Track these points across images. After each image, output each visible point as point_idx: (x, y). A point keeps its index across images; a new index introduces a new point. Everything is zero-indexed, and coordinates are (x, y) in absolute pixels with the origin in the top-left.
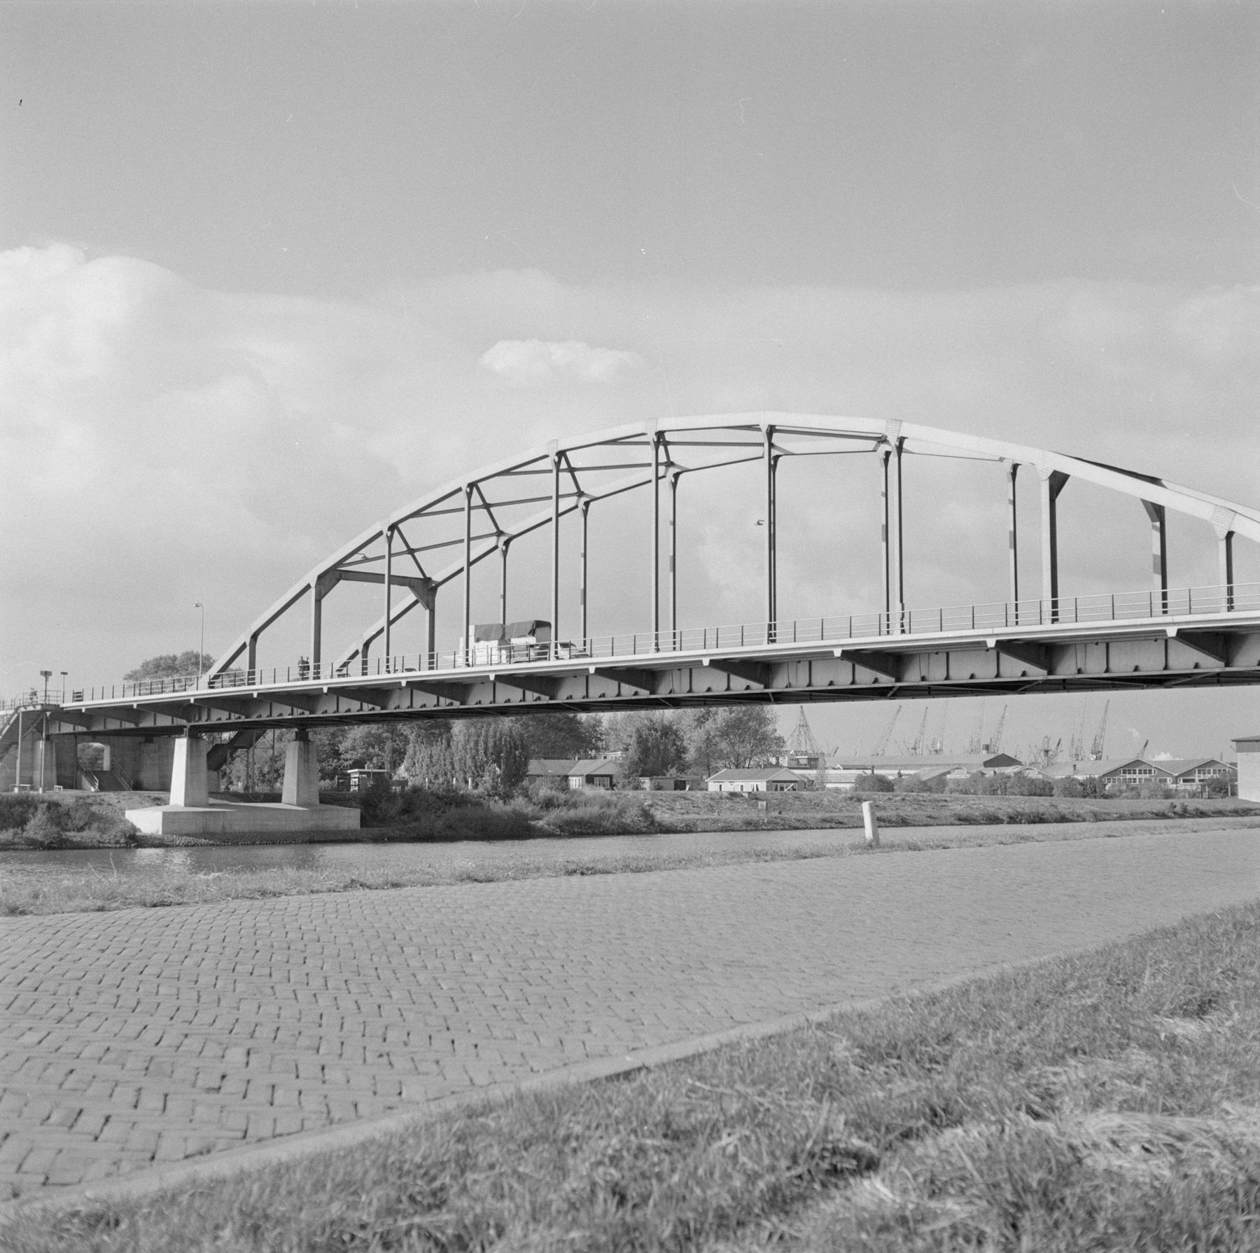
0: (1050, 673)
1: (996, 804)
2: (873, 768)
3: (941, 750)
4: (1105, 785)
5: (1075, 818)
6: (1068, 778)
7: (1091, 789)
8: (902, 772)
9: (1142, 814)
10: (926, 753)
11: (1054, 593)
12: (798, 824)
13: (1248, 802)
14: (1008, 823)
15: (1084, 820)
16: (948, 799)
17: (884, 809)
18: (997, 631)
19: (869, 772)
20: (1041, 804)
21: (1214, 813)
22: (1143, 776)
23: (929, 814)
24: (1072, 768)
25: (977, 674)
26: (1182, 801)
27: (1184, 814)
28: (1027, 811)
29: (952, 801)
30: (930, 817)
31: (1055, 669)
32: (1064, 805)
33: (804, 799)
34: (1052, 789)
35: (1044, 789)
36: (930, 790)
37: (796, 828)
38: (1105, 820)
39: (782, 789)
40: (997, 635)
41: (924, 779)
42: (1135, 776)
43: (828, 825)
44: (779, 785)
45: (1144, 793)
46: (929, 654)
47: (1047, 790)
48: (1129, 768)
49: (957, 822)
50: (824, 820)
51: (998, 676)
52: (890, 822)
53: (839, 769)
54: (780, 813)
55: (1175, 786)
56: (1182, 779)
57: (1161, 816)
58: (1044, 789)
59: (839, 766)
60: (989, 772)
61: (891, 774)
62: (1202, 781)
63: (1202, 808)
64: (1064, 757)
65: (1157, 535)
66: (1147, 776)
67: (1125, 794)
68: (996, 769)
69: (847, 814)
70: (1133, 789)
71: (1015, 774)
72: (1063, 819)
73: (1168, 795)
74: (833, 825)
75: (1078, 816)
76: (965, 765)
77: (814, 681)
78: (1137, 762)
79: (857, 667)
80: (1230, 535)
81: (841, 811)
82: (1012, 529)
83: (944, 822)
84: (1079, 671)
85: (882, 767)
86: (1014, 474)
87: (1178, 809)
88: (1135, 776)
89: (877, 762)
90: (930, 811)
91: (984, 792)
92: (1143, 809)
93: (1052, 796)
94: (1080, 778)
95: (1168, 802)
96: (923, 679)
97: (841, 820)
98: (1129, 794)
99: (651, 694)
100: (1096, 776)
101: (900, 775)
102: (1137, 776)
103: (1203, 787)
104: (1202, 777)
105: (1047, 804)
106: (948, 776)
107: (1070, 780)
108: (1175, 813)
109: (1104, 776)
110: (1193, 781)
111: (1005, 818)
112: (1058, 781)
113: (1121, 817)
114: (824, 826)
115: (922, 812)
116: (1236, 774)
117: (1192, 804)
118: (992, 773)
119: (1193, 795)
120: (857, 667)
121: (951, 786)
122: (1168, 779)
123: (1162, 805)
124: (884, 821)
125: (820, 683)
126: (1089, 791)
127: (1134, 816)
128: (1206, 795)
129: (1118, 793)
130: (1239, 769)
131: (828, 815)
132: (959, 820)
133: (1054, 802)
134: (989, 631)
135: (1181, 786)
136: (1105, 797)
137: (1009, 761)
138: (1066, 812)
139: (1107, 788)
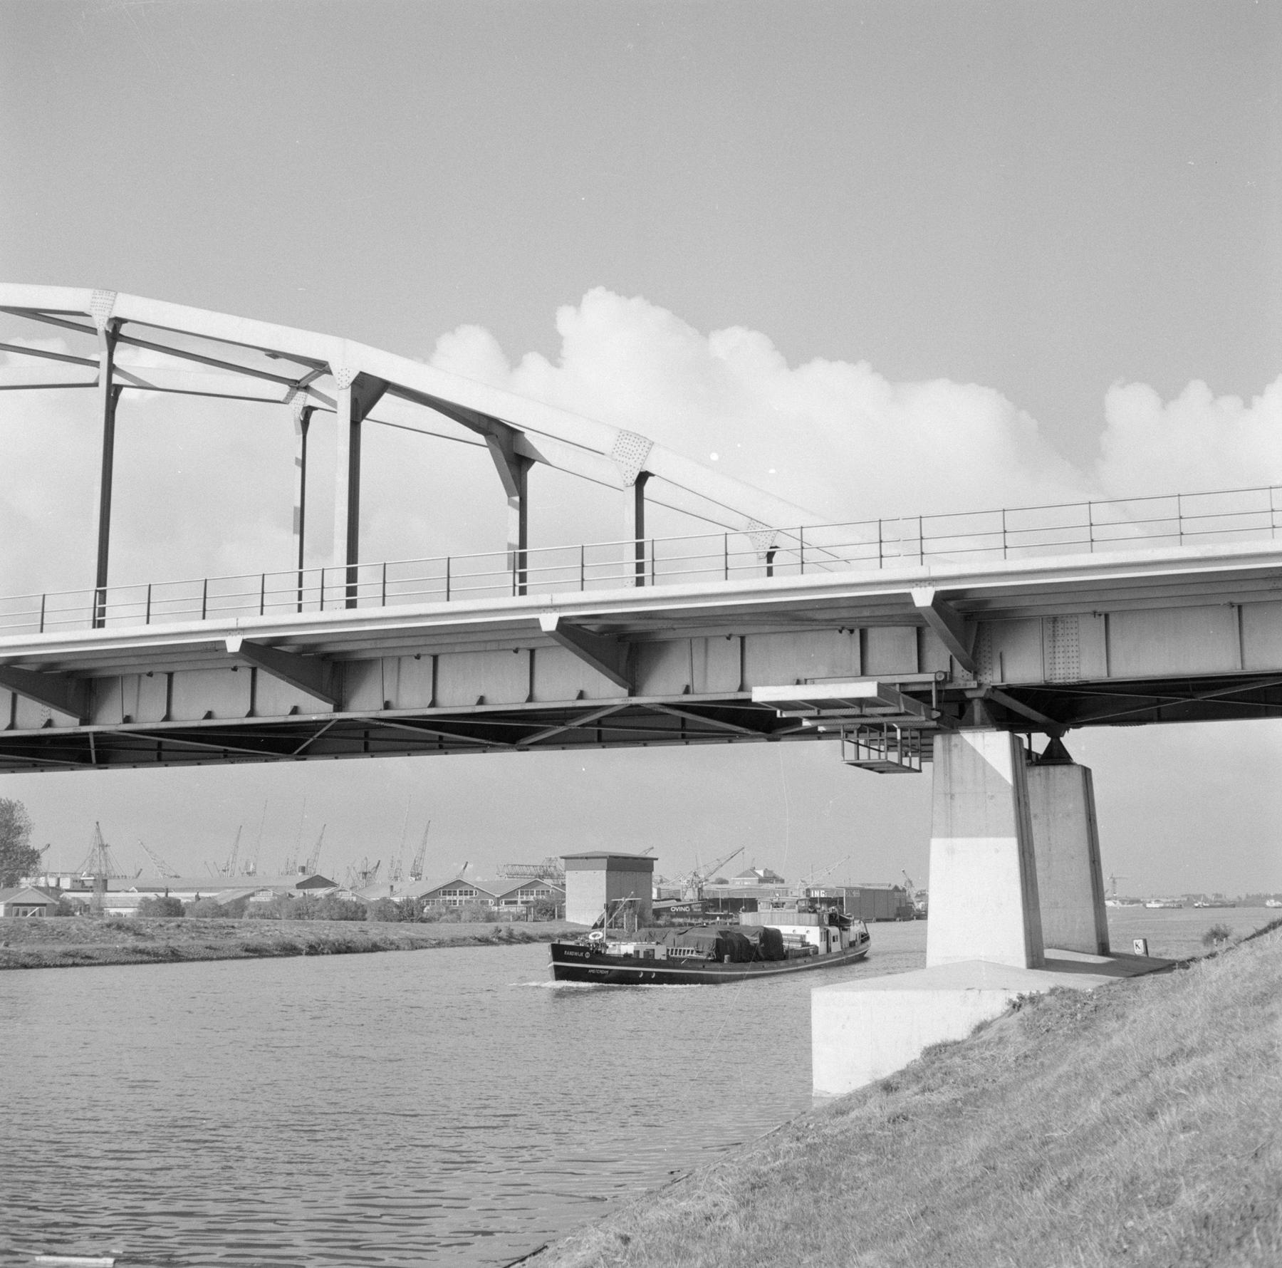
0: (338, 708)
1: (296, 931)
2: (167, 891)
3: (254, 872)
4: (423, 908)
5: (388, 946)
6: (384, 899)
7: (409, 912)
8: (201, 895)
9: (464, 939)
10: (237, 873)
11: (352, 555)
12: (28, 960)
13: (577, 925)
14: (308, 954)
15: (398, 948)
16: (236, 925)
17: (152, 938)
18: (560, 599)
19: (162, 895)
20: (349, 931)
21: (541, 937)
22: (464, 898)
23: (208, 944)
24: (389, 890)
25: (217, 712)
26: (507, 924)
27: (510, 939)
28: (332, 938)
29: (240, 928)
30: (210, 948)
31: (347, 702)
32: (374, 930)
33: (45, 926)
34: (365, 912)
35: (356, 912)
36: (226, 914)
37: (25, 966)
38: (422, 947)
39: (25, 913)
40: (243, 630)
41: (222, 903)
42: (455, 898)
43: (70, 961)
44: (22, 909)
45: (466, 915)
46: (140, 676)
47: (360, 914)
48: (448, 889)
49: (244, 954)
50: (66, 955)
51: (251, 714)
52: (156, 955)
53: (133, 891)
54: (7, 945)
55: (496, 908)
56: (503, 900)
57: (485, 941)
58: (355, 913)
59: (133, 888)
60: (299, 894)
61: (185, 897)
62: (527, 902)
63: (529, 932)
64: (382, 877)
65: (516, 514)
66: (468, 897)
67: (445, 917)
68: (306, 891)
69: (103, 945)
70: (452, 912)
71: (328, 896)
72: (375, 948)
73: (490, 918)
74: (78, 960)
75: (392, 943)
76: (270, 887)
77: (441, 697)
78: (459, 883)
79: (20, 698)
80: (643, 478)
81: (93, 941)
82: (299, 504)
83: (227, 954)
84: (387, 706)
85: (177, 890)
86: (305, 424)
87: (503, 934)
88: (455, 898)
89: (171, 883)
90: (211, 940)
91: (289, 917)
92: (466, 934)
93: (365, 920)
94: (397, 900)
95: (491, 926)
96: (127, 720)
97: (89, 953)
98: (449, 917)
99: (83, 723)
100: (414, 898)
101: (198, 898)
102: (458, 898)
103: (528, 909)
104: (525, 898)
105: (356, 930)
106: (252, 899)
107: (386, 901)
108: (500, 938)
109: (422, 897)
110: (515, 902)
111: (303, 947)
112: (370, 904)
113: (440, 944)
114: (63, 962)
115: (201, 942)
116: (564, 895)
117: (519, 928)
118: (302, 895)
119: (518, 918)
120: (20, 698)
121: (252, 910)
122: (490, 901)
123: (485, 929)
124: (148, 954)
125: (189, 714)
126: (406, 914)
127: (455, 943)
128: (531, 917)
129: (437, 916)
130: (567, 891)
131: (71, 947)
132: (247, 950)
133: (364, 928)
134: (230, 623)
135: (504, 908)
136: (423, 921)
137: (318, 882)
138: (377, 939)
139: (425, 910)
